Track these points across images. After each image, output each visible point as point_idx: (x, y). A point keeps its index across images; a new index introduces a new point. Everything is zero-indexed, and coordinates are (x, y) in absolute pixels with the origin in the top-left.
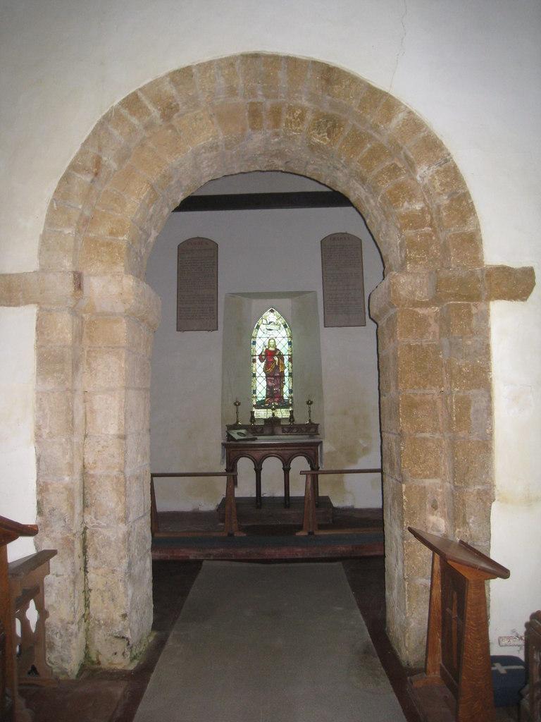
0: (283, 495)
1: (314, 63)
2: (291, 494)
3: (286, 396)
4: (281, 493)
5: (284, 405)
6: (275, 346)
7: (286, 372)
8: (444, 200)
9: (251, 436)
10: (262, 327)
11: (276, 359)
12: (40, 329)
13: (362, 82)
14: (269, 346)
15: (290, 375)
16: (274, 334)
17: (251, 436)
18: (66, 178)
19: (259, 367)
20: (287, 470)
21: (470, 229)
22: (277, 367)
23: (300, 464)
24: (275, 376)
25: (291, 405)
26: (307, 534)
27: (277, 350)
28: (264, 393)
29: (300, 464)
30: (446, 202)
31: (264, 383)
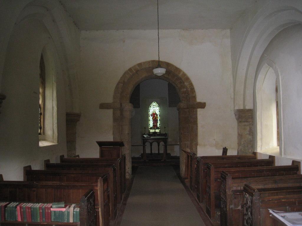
0: (158, 153)
1: (165, 62)
2: (160, 152)
3: (158, 126)
4: (157, 152)
5: (158, 128)
6: (155, 112)
7: (158, 119)
8: (189, 89)
9: (149, 137)
10: (152, 107)
11: (156, 116)
12: (114, 114)
13: (174, 66)
14: (154, 112)
15: (160, 120)
16: (155, 109)
17: (149, 137)
18: (118, 84)
19: (151, 118)
20: (159, 145)
21: (194, 95)
22: (156, 118)
23: (162, 143)
24: (155, 121)
25: (160, 128)
26: (164, 160)
27: (156, 113)
28: (152, 125)
29: (162, 143)
30: (190, 90)
31: (152, 122)
